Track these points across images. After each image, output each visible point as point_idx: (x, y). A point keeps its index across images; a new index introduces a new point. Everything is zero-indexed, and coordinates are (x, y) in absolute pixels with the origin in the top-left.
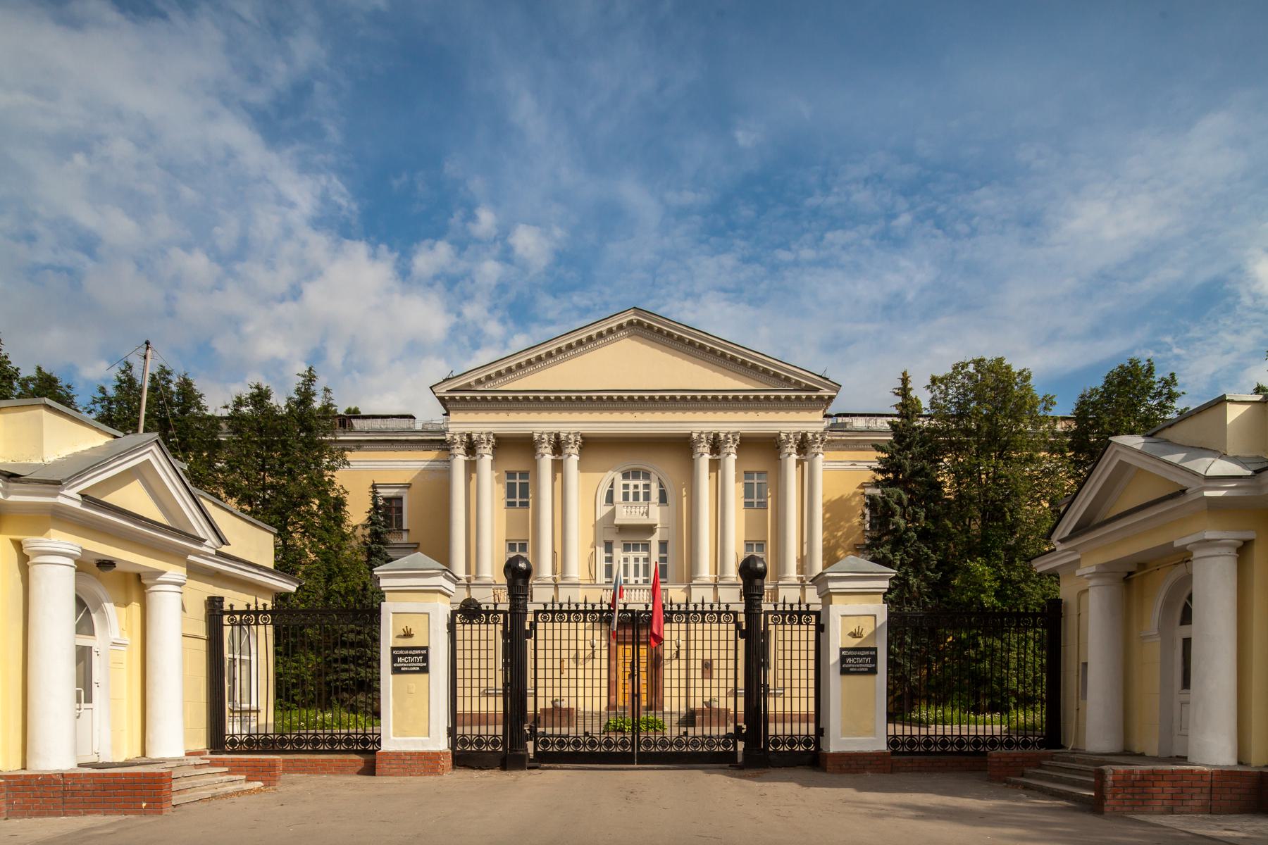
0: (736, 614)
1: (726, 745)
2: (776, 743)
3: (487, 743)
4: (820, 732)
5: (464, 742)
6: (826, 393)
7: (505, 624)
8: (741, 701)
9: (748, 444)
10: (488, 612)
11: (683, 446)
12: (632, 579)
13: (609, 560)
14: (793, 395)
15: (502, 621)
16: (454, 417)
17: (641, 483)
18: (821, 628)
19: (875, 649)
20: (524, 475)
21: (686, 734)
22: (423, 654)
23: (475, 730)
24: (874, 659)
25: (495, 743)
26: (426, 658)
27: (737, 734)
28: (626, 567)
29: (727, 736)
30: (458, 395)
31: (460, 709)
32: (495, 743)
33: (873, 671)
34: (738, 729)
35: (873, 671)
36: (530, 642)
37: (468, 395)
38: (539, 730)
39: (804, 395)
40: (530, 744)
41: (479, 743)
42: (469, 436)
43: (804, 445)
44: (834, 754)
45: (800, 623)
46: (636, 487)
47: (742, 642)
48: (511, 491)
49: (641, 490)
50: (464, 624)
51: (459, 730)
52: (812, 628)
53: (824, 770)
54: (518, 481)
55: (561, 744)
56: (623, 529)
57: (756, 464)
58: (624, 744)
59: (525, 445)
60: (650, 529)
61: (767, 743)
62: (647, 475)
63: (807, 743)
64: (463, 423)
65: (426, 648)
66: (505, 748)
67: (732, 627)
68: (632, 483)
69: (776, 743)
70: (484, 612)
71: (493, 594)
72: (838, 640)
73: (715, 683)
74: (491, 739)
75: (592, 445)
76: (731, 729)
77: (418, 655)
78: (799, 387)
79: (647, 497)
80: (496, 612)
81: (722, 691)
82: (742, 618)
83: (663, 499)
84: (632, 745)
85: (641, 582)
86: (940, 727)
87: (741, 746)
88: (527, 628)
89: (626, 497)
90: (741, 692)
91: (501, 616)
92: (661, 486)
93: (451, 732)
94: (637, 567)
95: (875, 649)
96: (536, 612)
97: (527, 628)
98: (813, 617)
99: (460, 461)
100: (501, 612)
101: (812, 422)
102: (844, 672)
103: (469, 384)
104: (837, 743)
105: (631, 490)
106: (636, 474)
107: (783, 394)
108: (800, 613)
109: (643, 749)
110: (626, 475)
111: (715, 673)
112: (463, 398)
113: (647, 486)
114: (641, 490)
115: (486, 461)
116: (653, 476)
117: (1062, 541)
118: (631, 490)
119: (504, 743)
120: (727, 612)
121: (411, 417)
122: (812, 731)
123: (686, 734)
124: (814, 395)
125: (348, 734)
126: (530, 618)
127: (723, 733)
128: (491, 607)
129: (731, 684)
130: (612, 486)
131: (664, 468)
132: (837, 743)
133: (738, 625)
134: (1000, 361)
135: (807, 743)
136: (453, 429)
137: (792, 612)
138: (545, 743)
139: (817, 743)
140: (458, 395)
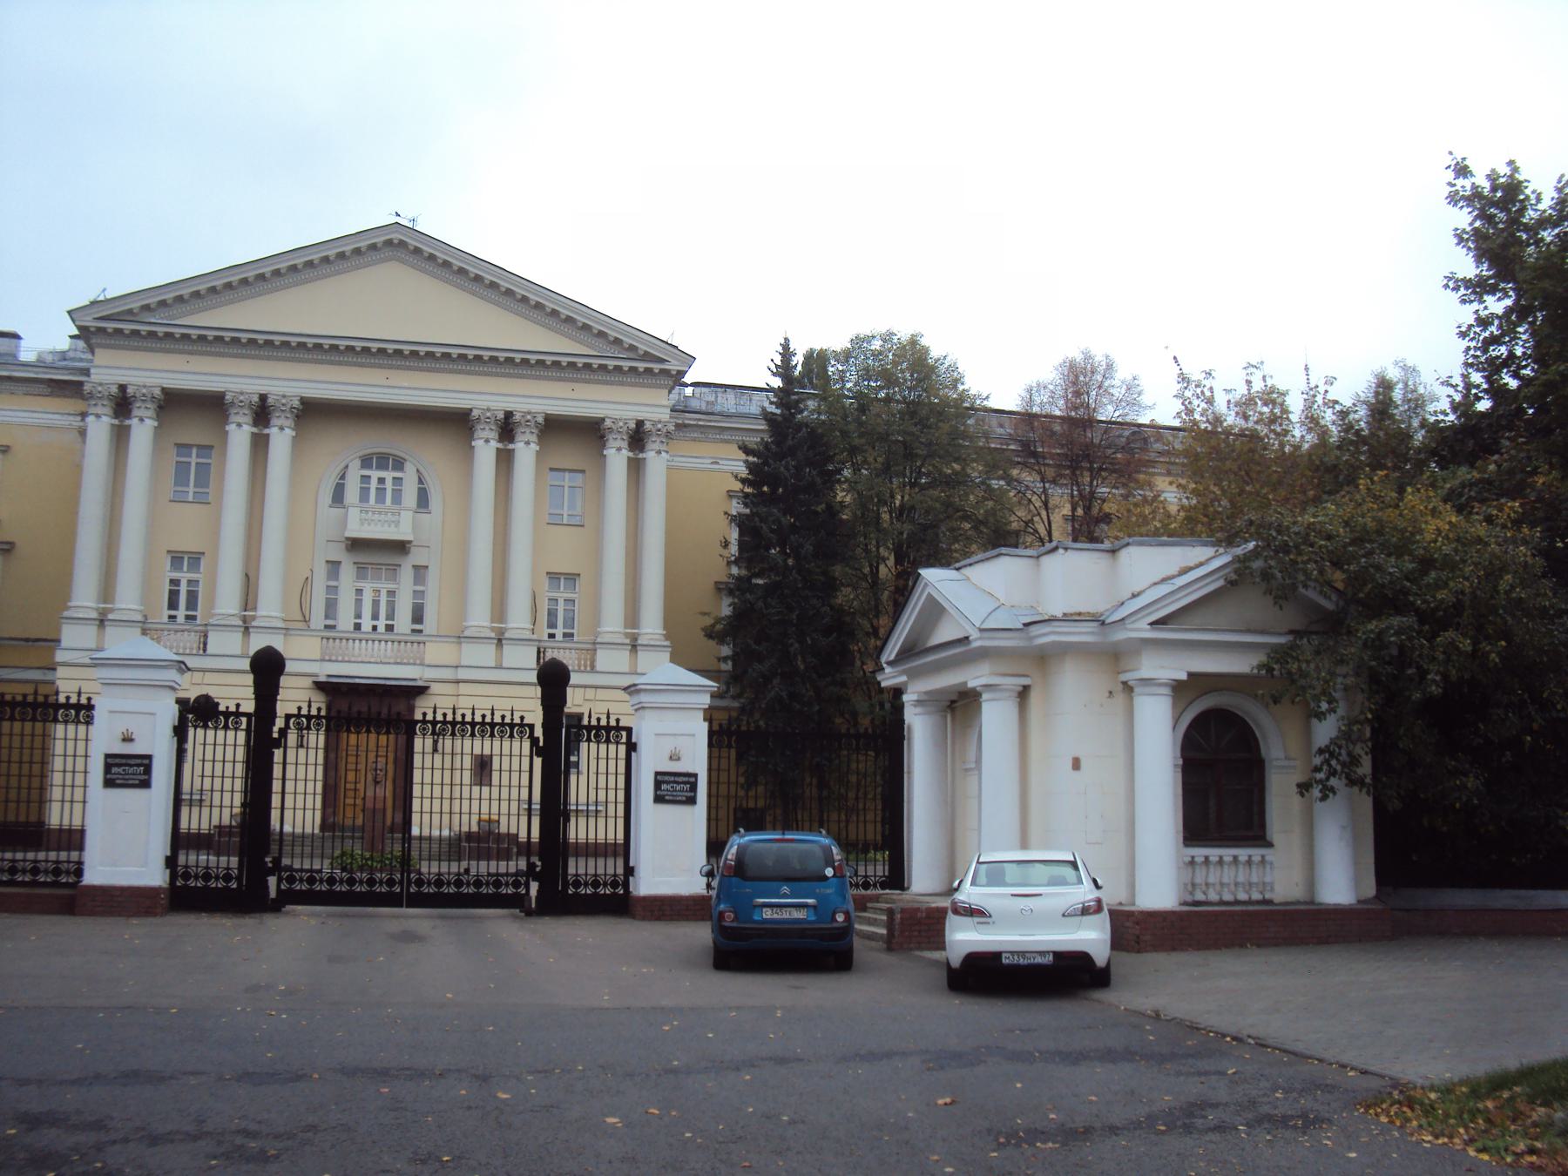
0: (532, 727)
1: (516, 884)
2: (577, 884)
3: (217, 878)
4: (629, 871)
5: (186, 876)
6: (673, 366)
7: (248, 730)
8: (536, 822)
9: (555, 428)
10: (227, 714)
11: (459, 423)
12: (367, 624)
13: (333, 590)
14: (626, 365)
15: (244, 726)
16: (103, 357)
17: (389, 475)
18: (632, 747)
19: (695, 776)
20: (205, 449)
21: (467, 871)
22: (146, 762)
23: (53, 855)
24: (694, 787)
25: (227, 878)
26: (148, 770)
27: (531, 872)
28: (359, 602)
29: (518, 873)
30: (110, 326)
31: (184, 825)
32: (227, 878)
33: (692, 801)
34: (531, 866)
35: (692, 801)
36: (278, 754)
37: (127, 327)
38: (286, 861)
39: (641, 366)
40: (272, 881)
41: (207, 877)
42: (123, 388)
43: (638, 437)
44: (645, 899)
45: (608, 741)
46: (381, 480)
47: (538, 761)
48: (182, 470)
49: (389, 485)
50: (196, 727)
51: (182, 859)
52: (622, 748)
53: (633, 917)
54: (194, 460)
55: (311, 881)
56: (356, 545)
57: (569, 455)
58: (391, 883)
59: (213, 406)
60: (401, 547)
61: (566, 884)
62: (399, 464)
63: (615, 884)
64: (113, 369)
65: (149, 757)
66: (240, 884)
67: (527, 745)
68: (375, 474)
69: (577, 884)
70: (222, 713)
71: (238, 693)
72: (649, 763)
73: (495, 790)
74: (222, 873)
75: (312, 412)
76: (523, 864)
77: (138, 765)
78: (647, 357)
79: (397, 496)
80: (238, 714)
81: (510, 801)
82: (539, 732)
83: (423, 500)
84: (401, 883)
85: (381, 629)
86: (435, 864)
87: (534, 887)
88: (275, 735)
89: (364, 493)
90: (536, 807)
91: (244, 720)
92: (420, 482)
93: (171, 862)
94: (376, 603)
95: (695, 776)
96: (288, 717)
97: (275, 735)
98: (624, 734)
99: (100, 427)
100: (244, 714)
101: (652, 406)
102: (659, 799)
103: (130, 312)
104: (647, 884)
105: (374, 484)
106: (383, 461)
107: (611, 363)
108: (608, 728)
109: (413, 889)
110: (366, 462)
111: (495, 775)
112: (119, 332)
113: (398, 481)
114: (389, 485)
115: (142, 430)
116: (410, 468)
117: (890, 663)
118: (374, 484)
119: (239, 879)
120: (522, 725)
121: (16, 336)
122: (620, 871)
123: (467, 871)
124: (656, 367)
125: (58, 862)
126: (280, 723)
127: (512, 870)
128: (232, 709)
129: (525, 795)
130: (343, 477)
131: (426, 456)
132: (647, 884)
133: (534, 741)
134: (913, 342)
135: (615, 884)
136: (97, 376)
137: (598, 728)
138: (291, 880)
139: (626, 885)
140: (110, 326)
